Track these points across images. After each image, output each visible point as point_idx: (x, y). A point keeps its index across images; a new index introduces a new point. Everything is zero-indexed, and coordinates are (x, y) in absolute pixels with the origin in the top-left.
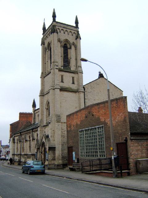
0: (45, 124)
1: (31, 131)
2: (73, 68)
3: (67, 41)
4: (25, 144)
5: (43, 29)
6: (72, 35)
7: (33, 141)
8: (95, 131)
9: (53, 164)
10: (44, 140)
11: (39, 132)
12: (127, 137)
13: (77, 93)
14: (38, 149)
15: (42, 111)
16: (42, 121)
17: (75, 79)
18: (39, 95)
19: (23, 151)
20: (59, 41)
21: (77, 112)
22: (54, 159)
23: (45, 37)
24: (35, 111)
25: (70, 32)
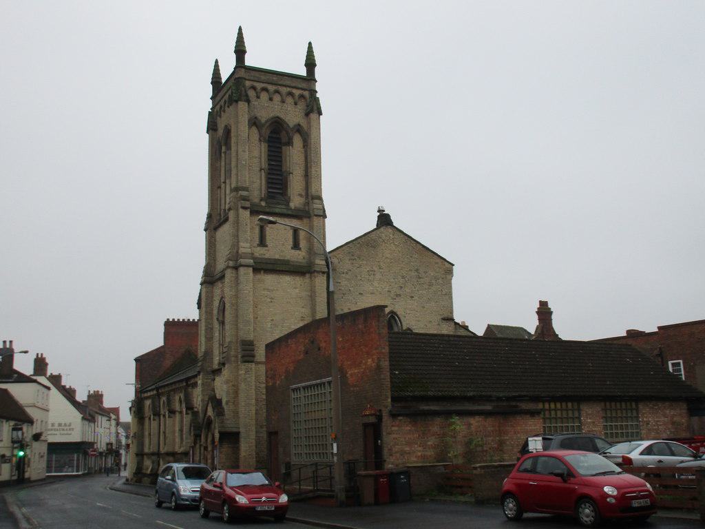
2: (296, 202)
5: (212, 83)
12: (383, 409)
13: (308, 276)
17: (302, 235)
18: (199, 280)
23: (218, 107)
25: (291, 94)
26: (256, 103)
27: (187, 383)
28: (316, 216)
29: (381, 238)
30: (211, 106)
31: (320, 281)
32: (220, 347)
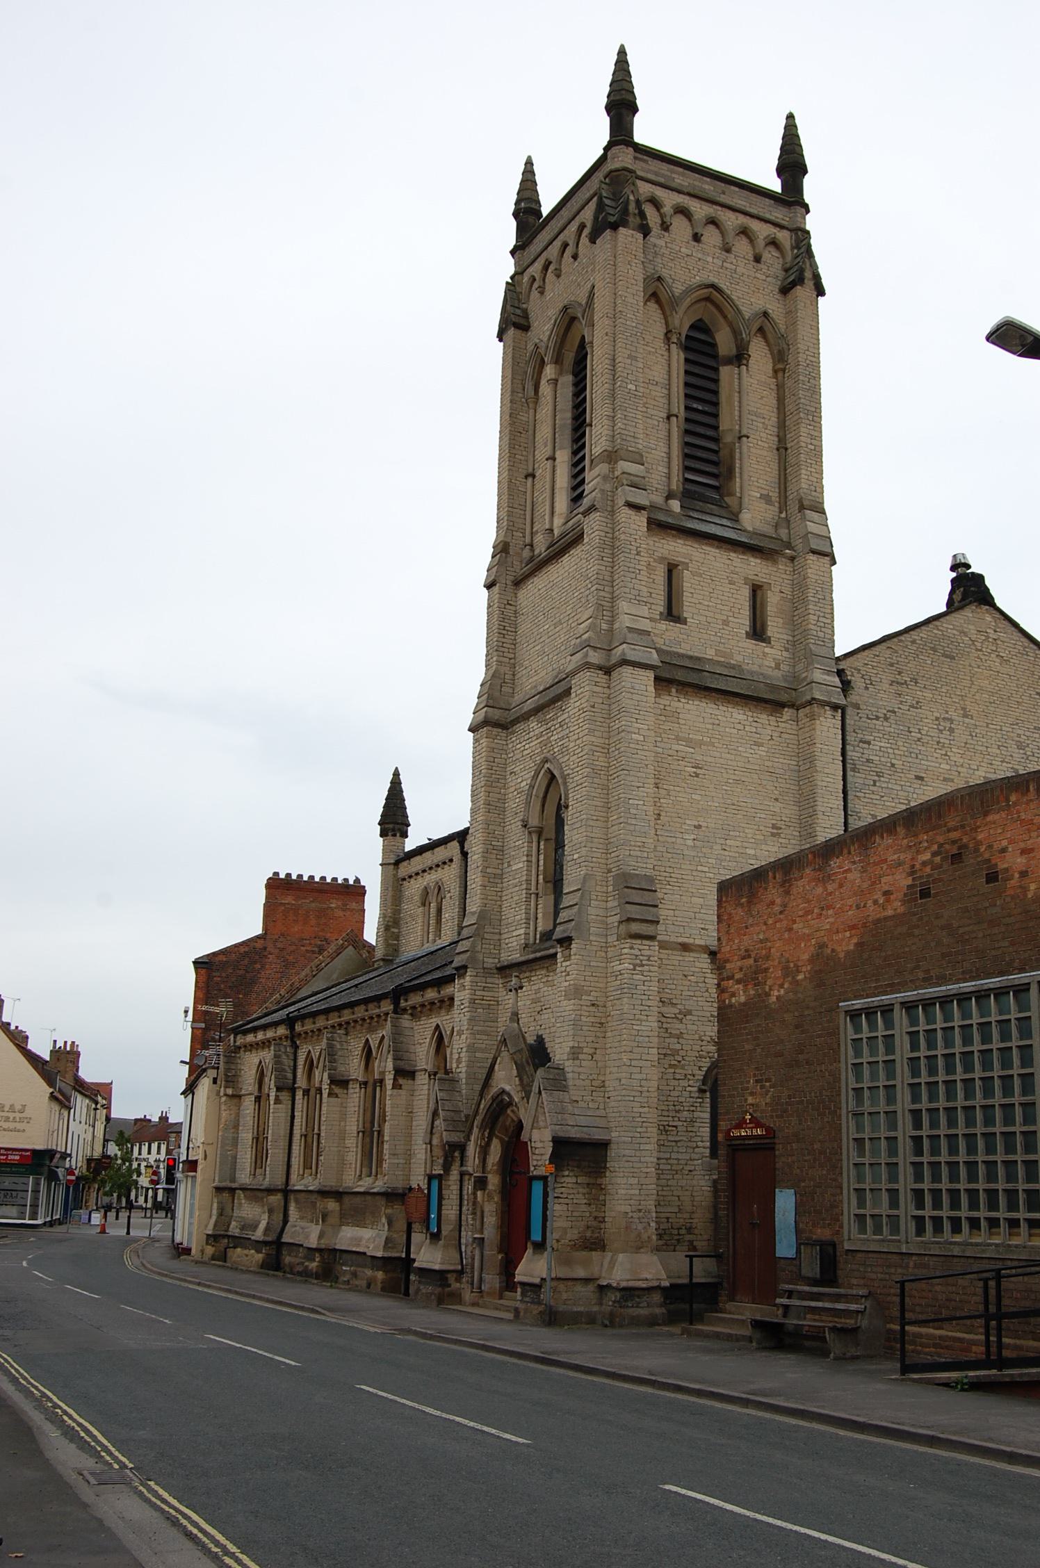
0: (512, 950)
1: (387, 1006)
3: (712, 295)
4: (328, 1106)
5: (516, 215)
6: (757, 259)
7: (396, 1086)
8: (881, 1031)
9: (587, 1281)
10: (505, 1079)
11: (458, 1020)
13: (788, 713)
14: (454, 1151)
15: (496, 850)
16: (489, 920)
17: (773, 600)
18: (468, 718)
19: (307, 1165)
20: (654, 296)
21: (786, 867)
22: (594, 1243)
23: (536, 269)
24: (397, 863)
25: (744, 232)
26: (661, 242)
27: (396, 1004)
28: (814, 552)
29: (965, 634)
30: (512, 271)
31: (827, 728)
32: (528, 900)
